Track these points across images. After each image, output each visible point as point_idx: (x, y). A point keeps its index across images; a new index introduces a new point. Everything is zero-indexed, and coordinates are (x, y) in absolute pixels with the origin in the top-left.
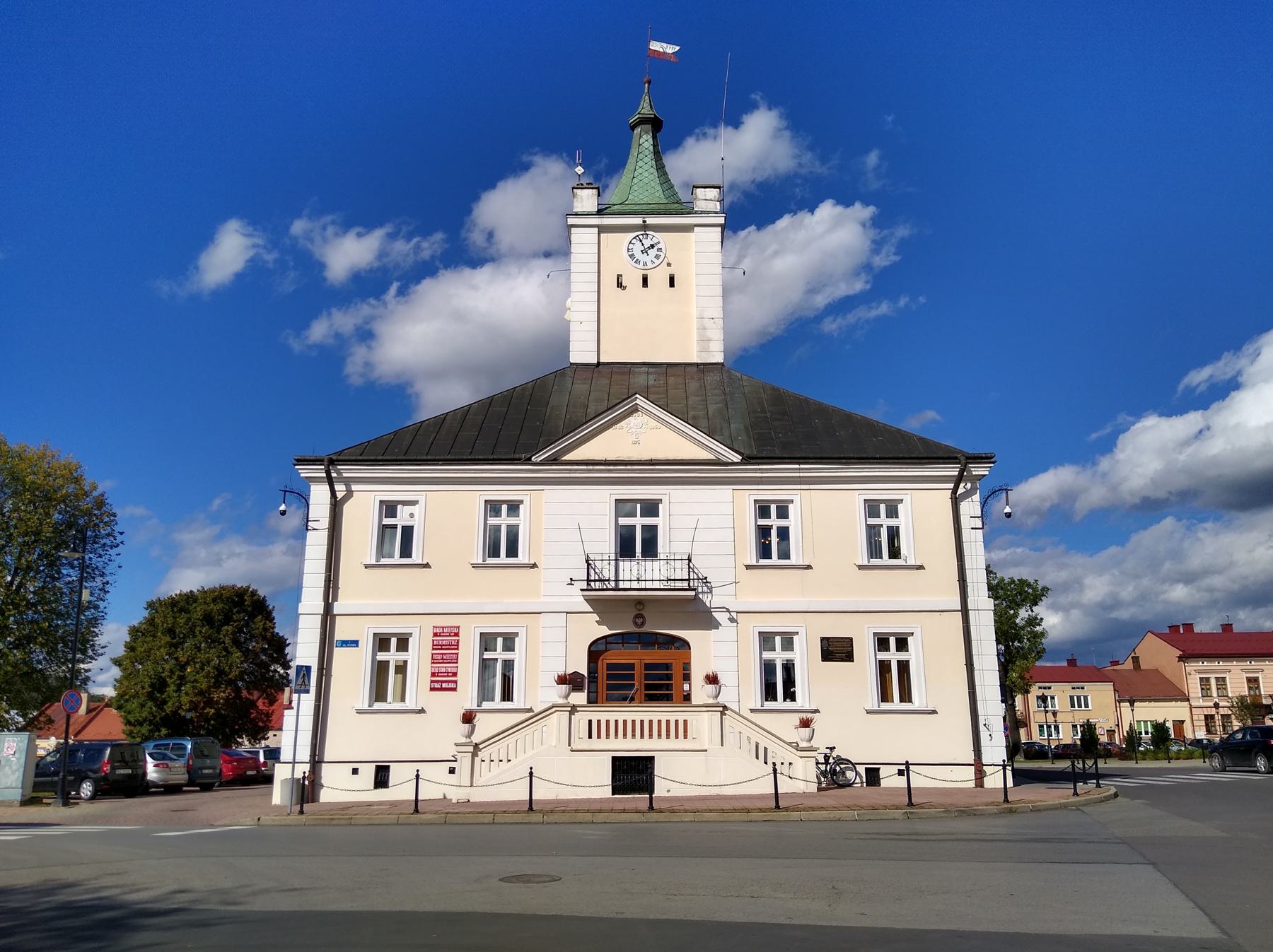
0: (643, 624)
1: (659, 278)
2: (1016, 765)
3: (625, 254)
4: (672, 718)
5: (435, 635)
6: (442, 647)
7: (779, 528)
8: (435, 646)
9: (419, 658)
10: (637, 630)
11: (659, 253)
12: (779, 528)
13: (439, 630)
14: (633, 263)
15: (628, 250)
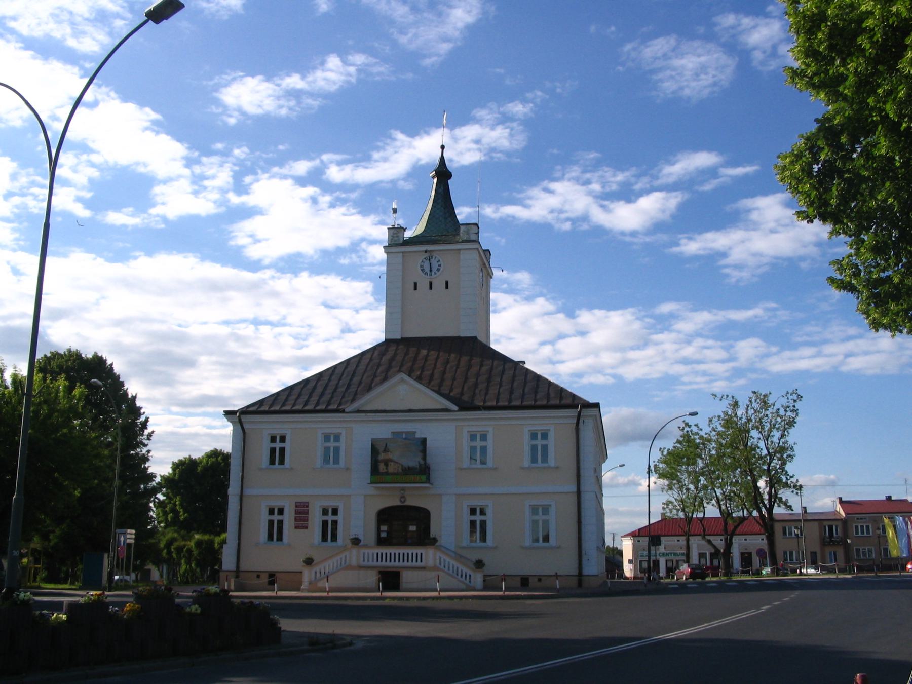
0: (404, 501)
1: (439, 284)
2: (232, 587)
3: (419, 269)
4: (397, 552)
5: (296, 506)
6: (300, 513)
7: (481, 447)
8: (296, 512)
9: (288, 519)
10: (402, 504)
11: (439, 268)
12: (481, 447)
13: (299, 504)
14: (423, 275)
15: (421, 266)
